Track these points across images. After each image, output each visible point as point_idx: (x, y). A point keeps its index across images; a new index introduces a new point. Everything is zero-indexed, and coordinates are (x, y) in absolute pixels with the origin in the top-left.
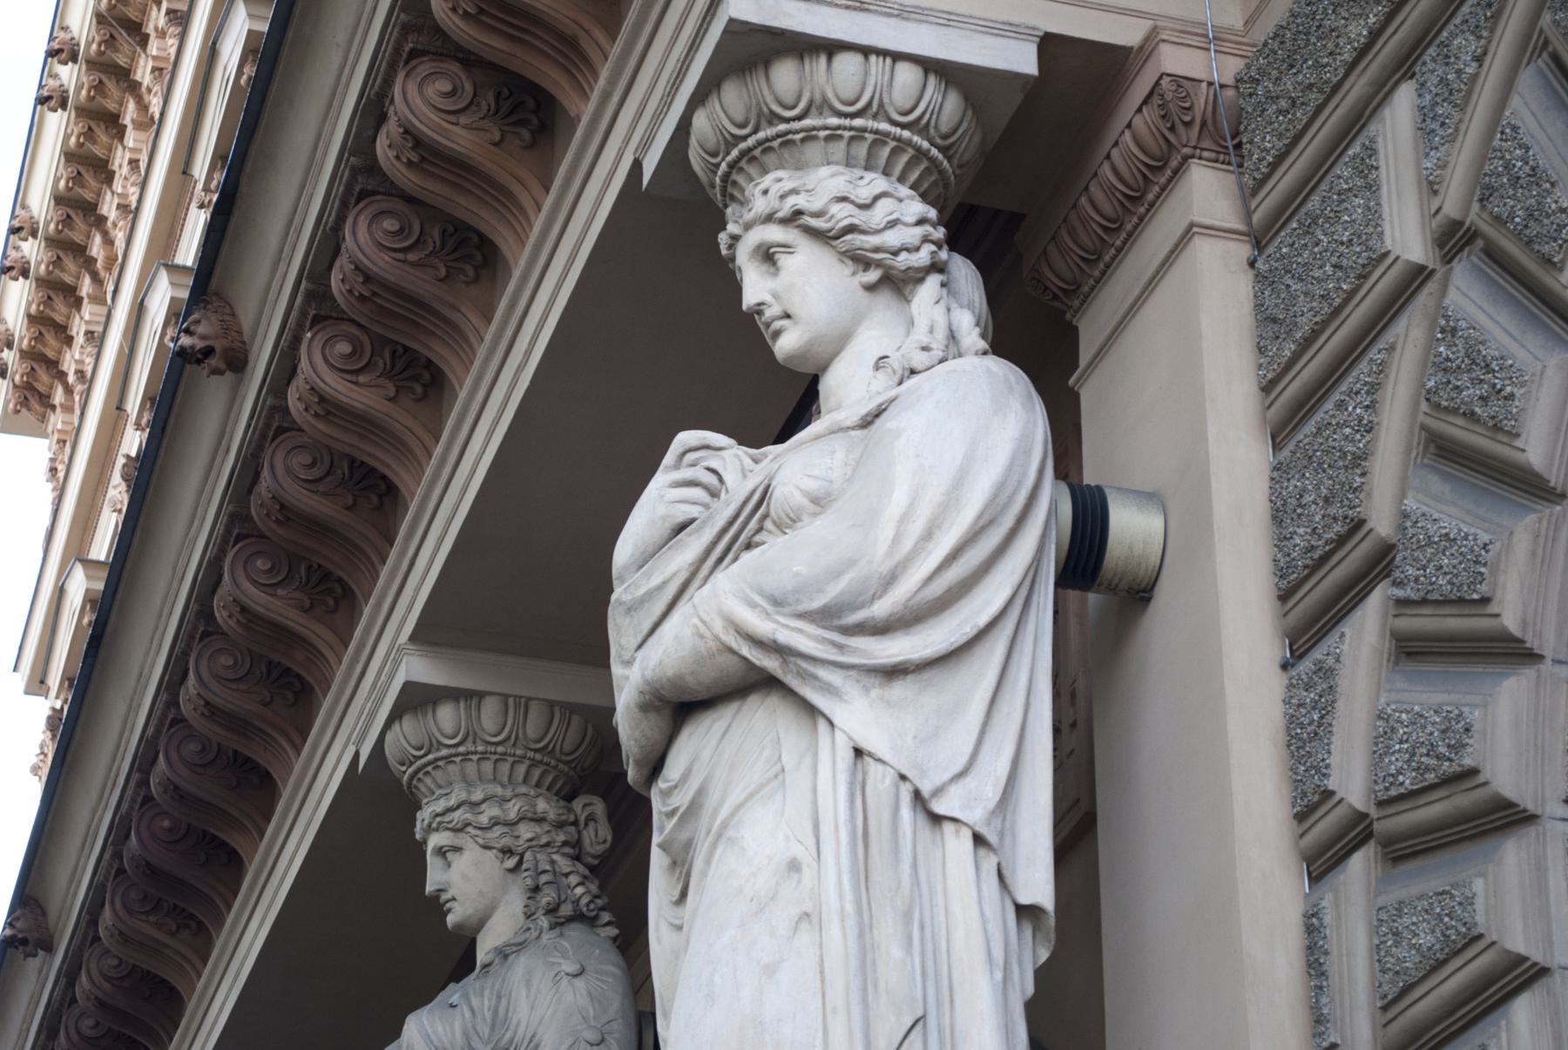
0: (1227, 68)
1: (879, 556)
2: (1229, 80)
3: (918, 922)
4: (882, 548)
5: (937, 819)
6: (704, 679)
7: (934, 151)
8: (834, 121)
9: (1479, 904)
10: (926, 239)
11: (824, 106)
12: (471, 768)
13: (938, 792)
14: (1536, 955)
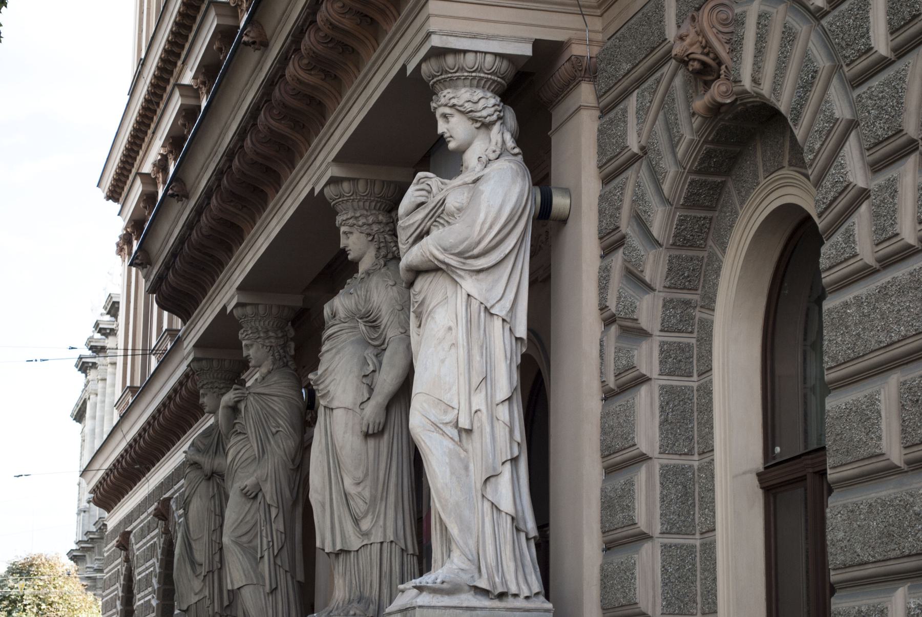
0: (596, 50)
1: (475, 236)
2: (594, 55)
3: (486, 349)
4: (476, 233)
5: (492, 315)
6: (424, 267)
7: (499, 80)
8: (466, 74)
9: (635, 358)
10: (496, 111)
11: (462, 69)
12: (355, 204)
13: (492, 306)
14: (648, 375)
